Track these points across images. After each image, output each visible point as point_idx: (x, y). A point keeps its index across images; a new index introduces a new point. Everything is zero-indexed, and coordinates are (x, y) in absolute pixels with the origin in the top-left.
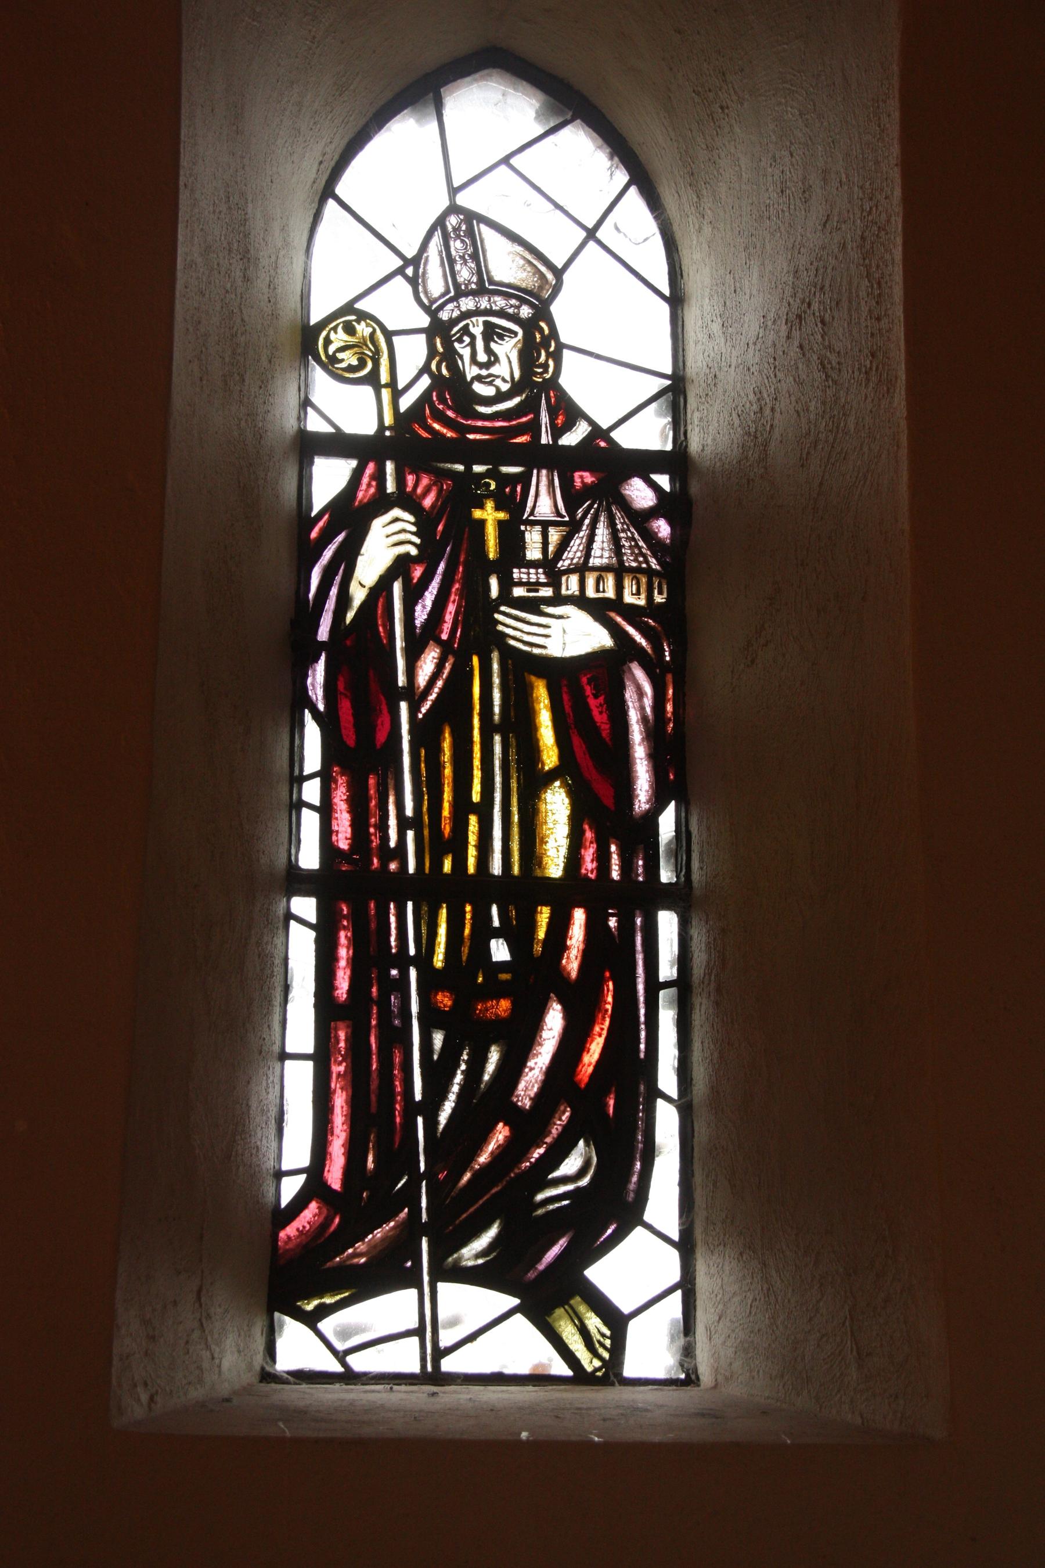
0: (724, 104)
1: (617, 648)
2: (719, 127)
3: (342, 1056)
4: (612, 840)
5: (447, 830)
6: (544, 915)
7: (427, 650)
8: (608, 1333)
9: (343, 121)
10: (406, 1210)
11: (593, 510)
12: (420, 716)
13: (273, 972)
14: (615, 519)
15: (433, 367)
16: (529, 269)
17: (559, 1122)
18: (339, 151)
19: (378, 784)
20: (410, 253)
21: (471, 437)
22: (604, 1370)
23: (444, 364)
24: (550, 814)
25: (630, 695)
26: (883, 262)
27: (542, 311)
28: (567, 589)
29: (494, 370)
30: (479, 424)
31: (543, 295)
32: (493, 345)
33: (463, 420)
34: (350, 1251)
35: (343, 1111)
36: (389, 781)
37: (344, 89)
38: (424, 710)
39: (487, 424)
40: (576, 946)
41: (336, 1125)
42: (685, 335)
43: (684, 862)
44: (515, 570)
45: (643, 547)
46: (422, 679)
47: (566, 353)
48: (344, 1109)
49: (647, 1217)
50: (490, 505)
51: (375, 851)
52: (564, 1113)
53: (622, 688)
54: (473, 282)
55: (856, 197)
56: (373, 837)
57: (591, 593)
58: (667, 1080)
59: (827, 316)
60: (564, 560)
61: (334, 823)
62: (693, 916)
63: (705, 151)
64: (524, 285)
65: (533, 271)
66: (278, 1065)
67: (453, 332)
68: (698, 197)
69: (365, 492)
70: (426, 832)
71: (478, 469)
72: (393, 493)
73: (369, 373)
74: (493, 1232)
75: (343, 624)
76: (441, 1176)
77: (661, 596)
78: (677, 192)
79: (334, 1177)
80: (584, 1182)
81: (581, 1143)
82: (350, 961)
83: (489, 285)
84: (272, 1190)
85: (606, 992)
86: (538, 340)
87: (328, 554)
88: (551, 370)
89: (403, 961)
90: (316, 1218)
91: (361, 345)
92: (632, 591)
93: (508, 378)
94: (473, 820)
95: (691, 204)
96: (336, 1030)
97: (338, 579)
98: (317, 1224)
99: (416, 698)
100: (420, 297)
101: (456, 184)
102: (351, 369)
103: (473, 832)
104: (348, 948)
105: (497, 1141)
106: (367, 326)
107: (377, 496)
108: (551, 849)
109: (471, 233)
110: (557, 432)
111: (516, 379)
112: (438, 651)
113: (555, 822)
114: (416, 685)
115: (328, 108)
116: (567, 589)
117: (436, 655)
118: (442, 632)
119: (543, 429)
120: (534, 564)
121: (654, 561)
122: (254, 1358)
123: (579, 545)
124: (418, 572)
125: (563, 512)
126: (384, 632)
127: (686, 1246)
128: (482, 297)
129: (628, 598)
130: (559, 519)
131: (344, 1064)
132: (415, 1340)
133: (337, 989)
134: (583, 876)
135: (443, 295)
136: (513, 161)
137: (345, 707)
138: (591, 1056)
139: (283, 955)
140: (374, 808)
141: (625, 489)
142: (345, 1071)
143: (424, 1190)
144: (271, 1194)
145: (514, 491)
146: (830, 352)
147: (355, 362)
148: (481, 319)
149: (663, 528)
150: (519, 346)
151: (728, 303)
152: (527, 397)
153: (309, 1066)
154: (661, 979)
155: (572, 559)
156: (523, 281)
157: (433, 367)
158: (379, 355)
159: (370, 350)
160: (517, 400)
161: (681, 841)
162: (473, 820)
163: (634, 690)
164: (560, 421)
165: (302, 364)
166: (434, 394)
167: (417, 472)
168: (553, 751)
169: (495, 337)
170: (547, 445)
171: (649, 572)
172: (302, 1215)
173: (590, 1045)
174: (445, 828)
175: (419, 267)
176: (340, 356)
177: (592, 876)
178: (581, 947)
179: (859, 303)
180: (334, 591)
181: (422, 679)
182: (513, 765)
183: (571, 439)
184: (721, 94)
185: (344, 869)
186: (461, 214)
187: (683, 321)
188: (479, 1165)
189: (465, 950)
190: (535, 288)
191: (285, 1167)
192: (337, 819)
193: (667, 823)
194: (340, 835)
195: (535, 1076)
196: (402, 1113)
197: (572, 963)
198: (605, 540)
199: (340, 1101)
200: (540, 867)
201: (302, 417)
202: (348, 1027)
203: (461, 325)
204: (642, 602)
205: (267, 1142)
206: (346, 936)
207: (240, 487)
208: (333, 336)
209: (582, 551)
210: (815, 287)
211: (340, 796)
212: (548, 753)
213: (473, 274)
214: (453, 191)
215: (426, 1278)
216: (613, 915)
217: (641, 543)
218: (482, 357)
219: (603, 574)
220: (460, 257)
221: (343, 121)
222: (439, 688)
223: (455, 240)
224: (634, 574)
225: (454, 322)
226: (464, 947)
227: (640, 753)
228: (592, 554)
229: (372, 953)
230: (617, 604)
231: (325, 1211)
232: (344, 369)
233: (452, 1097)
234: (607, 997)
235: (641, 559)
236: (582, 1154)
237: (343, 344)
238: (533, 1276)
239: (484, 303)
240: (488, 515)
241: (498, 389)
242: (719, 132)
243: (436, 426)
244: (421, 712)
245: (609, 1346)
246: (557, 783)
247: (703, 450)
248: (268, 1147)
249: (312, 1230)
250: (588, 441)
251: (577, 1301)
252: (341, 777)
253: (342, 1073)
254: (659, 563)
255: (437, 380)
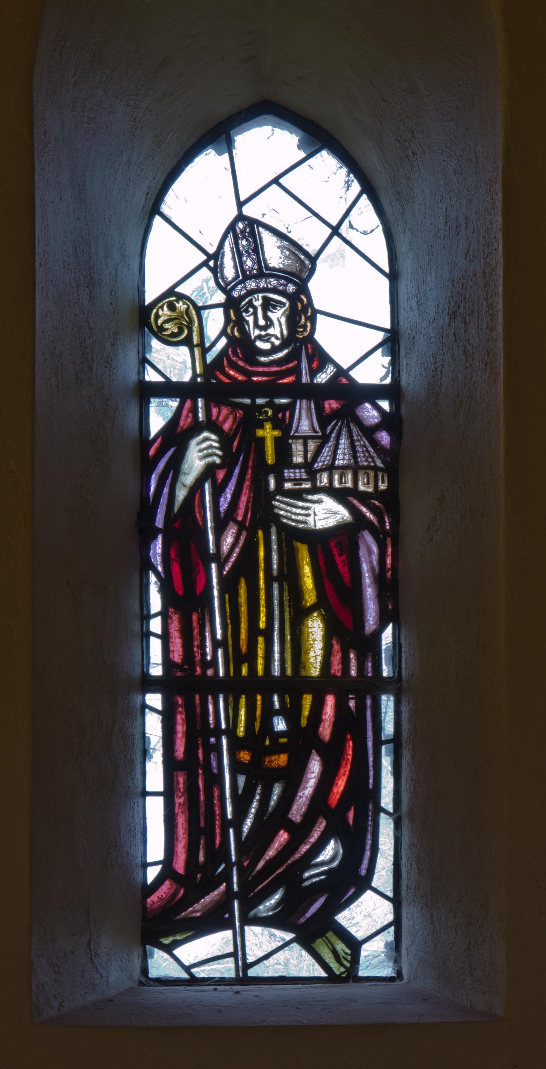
0: (414, 151)
1: (354, 522)
2: (412, 166)
3: (181, 792)
4: (351, 650)
5: (244, 649)
6: (307, 701)
7: (228, 528)
8: (348, 951)
9: (162, 163)
10: (224, 884)
11: (337, 427)
12: (225, 573)
13: (134, 744)
14: (352, 432)
15: (229, 331)
16: (293, 258)
17: (318, 829)
18: (161, 183)
19: (199, 619)
20: (211, 250)
21: (255, 379)
22: (346, 973)
23: (236, 328)
24: (311, 635)
25: (363, 553)
26: (494, 293)
27: (303, 289)
28: (321, 482)
29: (271, 331)
30: (261, 369)
31: (303, 276)
32: (269, 314)
33: (250, 367)
34: (191, 909)
35: (183, 827)
36: (206, 616)
37: (161, 143)
38: (227, 569)
39: (266, 369)
40: (329, 719)
41: (179, 835)
42: (398, 302)
43: (397, 663)
44: (286, 471)
45: (371, 451)
46: (225, 548)
47: (319, 316)
48: (184, 825)
49: (374, 884)
50: (268, 426)
51: (197, 663)
52: (321, 823)
53: (357, 548)
54: (255, 269)
55: (481, 243)
56: (196, 654)
57: (336, 484)
58: (387, 801)
59: (467, 319)
60: (318, 463)
61: (171, 645)
62: (403, 698)
63: (405, 180)
64: (289, 270)
65: (295, 259)
66: (141, 800)
67: (241, 306)
68: (403, 209)
69: (185, 422)
70: (231, 650)
71: (260, 401)
72: (203, 421)
73: (185, 337)
74: (277, 896)
75: (172, 512)
76: (245, 864)
77: (383, 485)
78: (391, 203)
79: (180, 865)
80: (335, 864)
81: (332, 842)
82: (184, 733)
83: (266, 271)
84: (141, 875)
85: (347, 748)
86: (299, 309)
87: (161, 465)
88: (308, 329)
89: (218, 732)
90: (169, 890)
91: (179, 317)
92: (364, 482)
93: (279, 335)
94: (261, 640)
95: (399, 212)
96: (177, 777)
97: (168, 482)
98: (170, 894)
99: (222, 560)
100: (219, 281)
101: (242, 198)
102: (173, 335)
103: (261, 648)
104: (183, 725)
105: (280, 842)
106: (183, 304)
107: (193, 424)
108: (312, 658)
109: (253, 234)
110: (313, 373)
111: (285, 337)
112: (236, 528)
113: (314, 640)
114: (222, 552)
115: (150, 158)
116: (321, 482)
117: (234, 531)
118: (238, 515)
119: (304, 372)
120: (298, 466)
121: (379, 461)
122: (133, 972)
123: (328, 452)
124: (221, 475)
125: (318, 429)
126: (200, 517)
127: (396, 901)
128: (261, 280)
129: (362, 488)
130: (315, 434)
131: (183, 798)
132: (231, 960)
133: (176, 752)
134: (332, 674)
135: (234, 279)
136: (281, 181)
137: (176, 569)
138: (338, 788)
139: (140, 732)
140: (196, 635)
141: (359, 411)
142: (184, 802)
143: (235, 872)
144: (140, 878)
145: (284, 416)
146: (469, 344)
147: (176, 330)
148: (260, 295)
149: (384, 438)
150: (287, 313)
151: (420, 289)
152: (293, 349)
153: (161, 800)
154: (383, 739)
155: (324, 462)
156: (289, 266)
157: (229, 331)
158: (192, 324)
159: (186, 321)
160: (285, 352)
161: (396, 650)
162: (261, 640)
163: (365, 550)
164: (315, 365)
165: (140, 333)
166: (230, 350)
167: (218, 405)
168: (312, 593)
169: (270, 307)
170: (307, 384)
171: (376, 469)
172: (161, 889)
173: (338, 781)
174: (242, 646)
175: (218, 260)
176: (167, 326)
177: (339, 674)
178: (332, 720)
179: (483, 316)
180: (166, 490)
181: (225, 548)
182: (286, 603)
183: (322, 378)
184: (412, 145)
185: (178, 675)
186: (246, 221)
187: (397, 292)
188: (269, 856)
189: (257, 725)
190: (297, 271)
191: (149, 860)
192: (173, 643)
193: (387, 636)
194: (175, 653)
195: (303, 802)
196: (220, 827)
197: (326, 730)
198: (346, 448)
199: (181, 820)
200: (304, 669)
201: (141, 372)
202: (184, 775)
203: (247, 300)
204: (370, 490)
205: (135, 848)
206: (181, 718)
207: (58, 162)
208: (160, 312)
209: (330, 456)
210: (462, 296)
211: (174, 628)
212: (309, 594)
213: (255, 263)
214: (240, 204)
215: (237, 924)
216: (352, 699)
217: (370, 449)
218: (262, 322)
219: (345, 471)
220: (246, 251)
221: (162, 163)
222: (237, 553)
223: (242, 240)
224: (365, 471)
225: (242, 298)
226: (257, 722)
227: (369, 592)
228: (337, 457)
229: (198, 728)
230: (354, 491)
231: (174, 886)
232: (168, 336)
233: (251, 816)
234: (349, 750)
235: (370, 460)
236: (333, 848)
237: (167, 317)
238: (303, 921)
239: (262, 284)
240: (267, 433)
241: (273, 344)
242: (413, 169)
243: (232, 373)
244: (225, 570)
245: (350, 960)
246: (315, 614)
247: (408, 386)
248: (136, 851)
249: (167, 897)
250: (334, 379)
251: (330, 935)
252: (174, 615)
253: (182, 803)
254: (383, 463)
255: (231, 339)
